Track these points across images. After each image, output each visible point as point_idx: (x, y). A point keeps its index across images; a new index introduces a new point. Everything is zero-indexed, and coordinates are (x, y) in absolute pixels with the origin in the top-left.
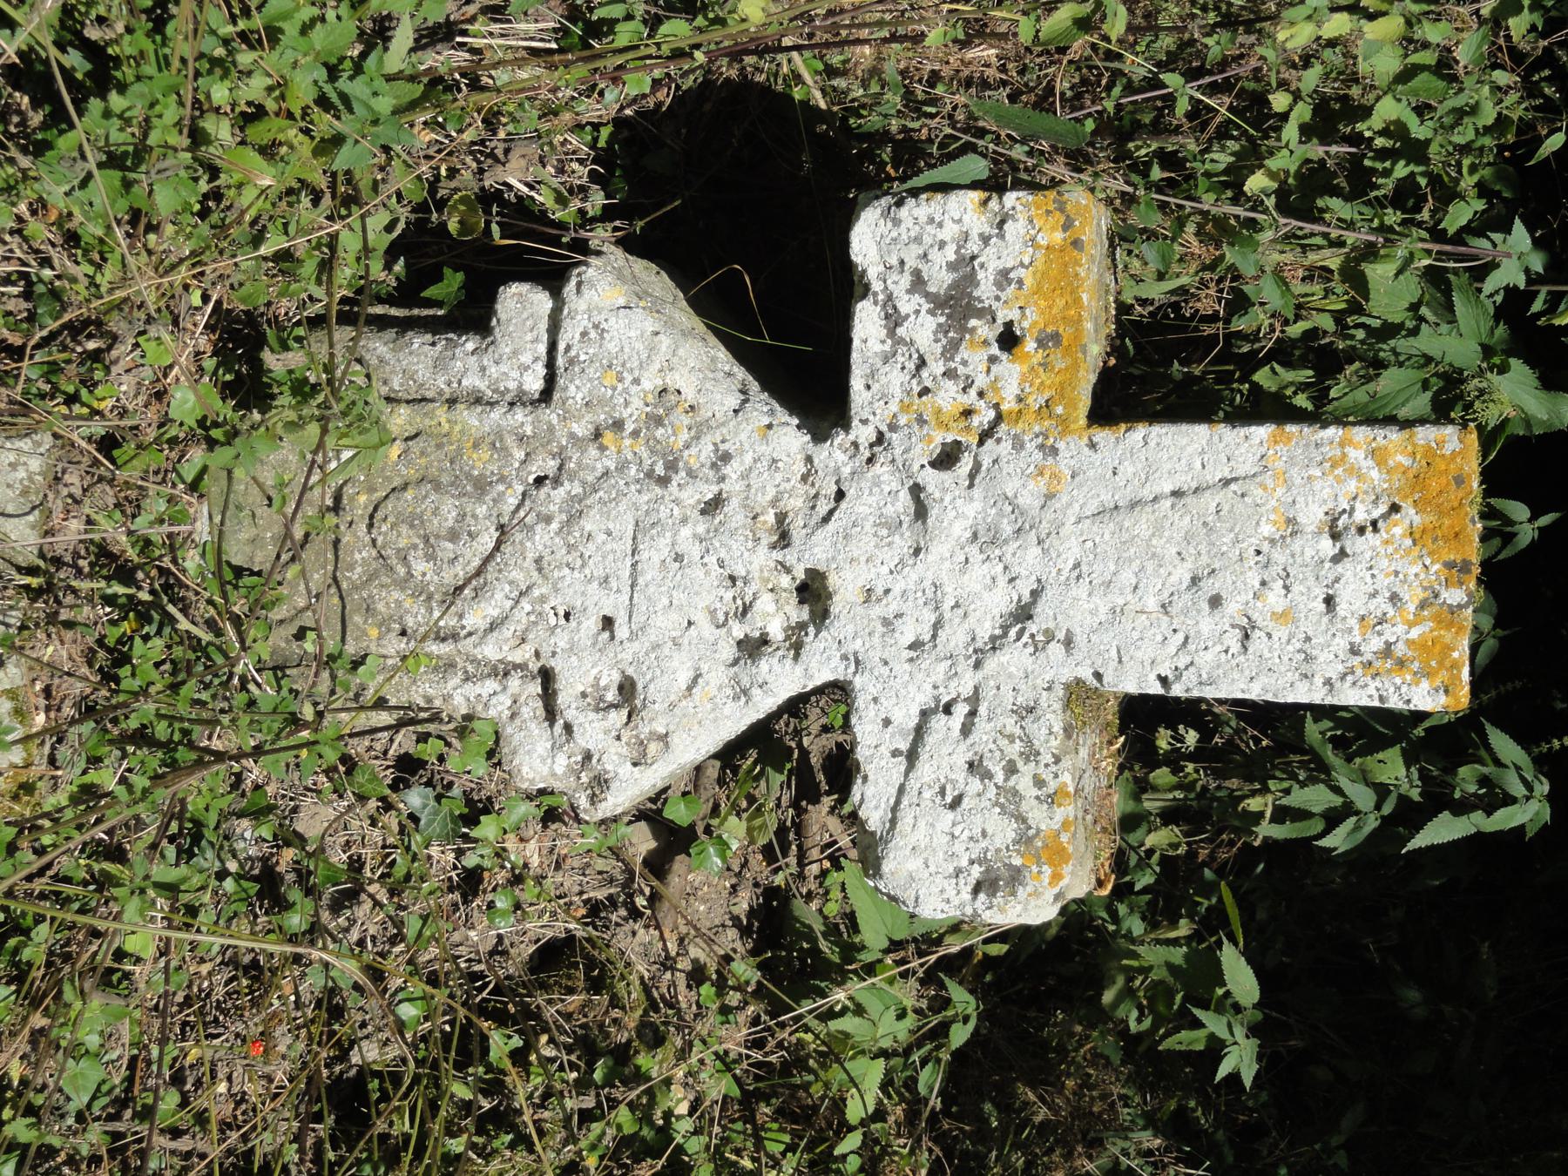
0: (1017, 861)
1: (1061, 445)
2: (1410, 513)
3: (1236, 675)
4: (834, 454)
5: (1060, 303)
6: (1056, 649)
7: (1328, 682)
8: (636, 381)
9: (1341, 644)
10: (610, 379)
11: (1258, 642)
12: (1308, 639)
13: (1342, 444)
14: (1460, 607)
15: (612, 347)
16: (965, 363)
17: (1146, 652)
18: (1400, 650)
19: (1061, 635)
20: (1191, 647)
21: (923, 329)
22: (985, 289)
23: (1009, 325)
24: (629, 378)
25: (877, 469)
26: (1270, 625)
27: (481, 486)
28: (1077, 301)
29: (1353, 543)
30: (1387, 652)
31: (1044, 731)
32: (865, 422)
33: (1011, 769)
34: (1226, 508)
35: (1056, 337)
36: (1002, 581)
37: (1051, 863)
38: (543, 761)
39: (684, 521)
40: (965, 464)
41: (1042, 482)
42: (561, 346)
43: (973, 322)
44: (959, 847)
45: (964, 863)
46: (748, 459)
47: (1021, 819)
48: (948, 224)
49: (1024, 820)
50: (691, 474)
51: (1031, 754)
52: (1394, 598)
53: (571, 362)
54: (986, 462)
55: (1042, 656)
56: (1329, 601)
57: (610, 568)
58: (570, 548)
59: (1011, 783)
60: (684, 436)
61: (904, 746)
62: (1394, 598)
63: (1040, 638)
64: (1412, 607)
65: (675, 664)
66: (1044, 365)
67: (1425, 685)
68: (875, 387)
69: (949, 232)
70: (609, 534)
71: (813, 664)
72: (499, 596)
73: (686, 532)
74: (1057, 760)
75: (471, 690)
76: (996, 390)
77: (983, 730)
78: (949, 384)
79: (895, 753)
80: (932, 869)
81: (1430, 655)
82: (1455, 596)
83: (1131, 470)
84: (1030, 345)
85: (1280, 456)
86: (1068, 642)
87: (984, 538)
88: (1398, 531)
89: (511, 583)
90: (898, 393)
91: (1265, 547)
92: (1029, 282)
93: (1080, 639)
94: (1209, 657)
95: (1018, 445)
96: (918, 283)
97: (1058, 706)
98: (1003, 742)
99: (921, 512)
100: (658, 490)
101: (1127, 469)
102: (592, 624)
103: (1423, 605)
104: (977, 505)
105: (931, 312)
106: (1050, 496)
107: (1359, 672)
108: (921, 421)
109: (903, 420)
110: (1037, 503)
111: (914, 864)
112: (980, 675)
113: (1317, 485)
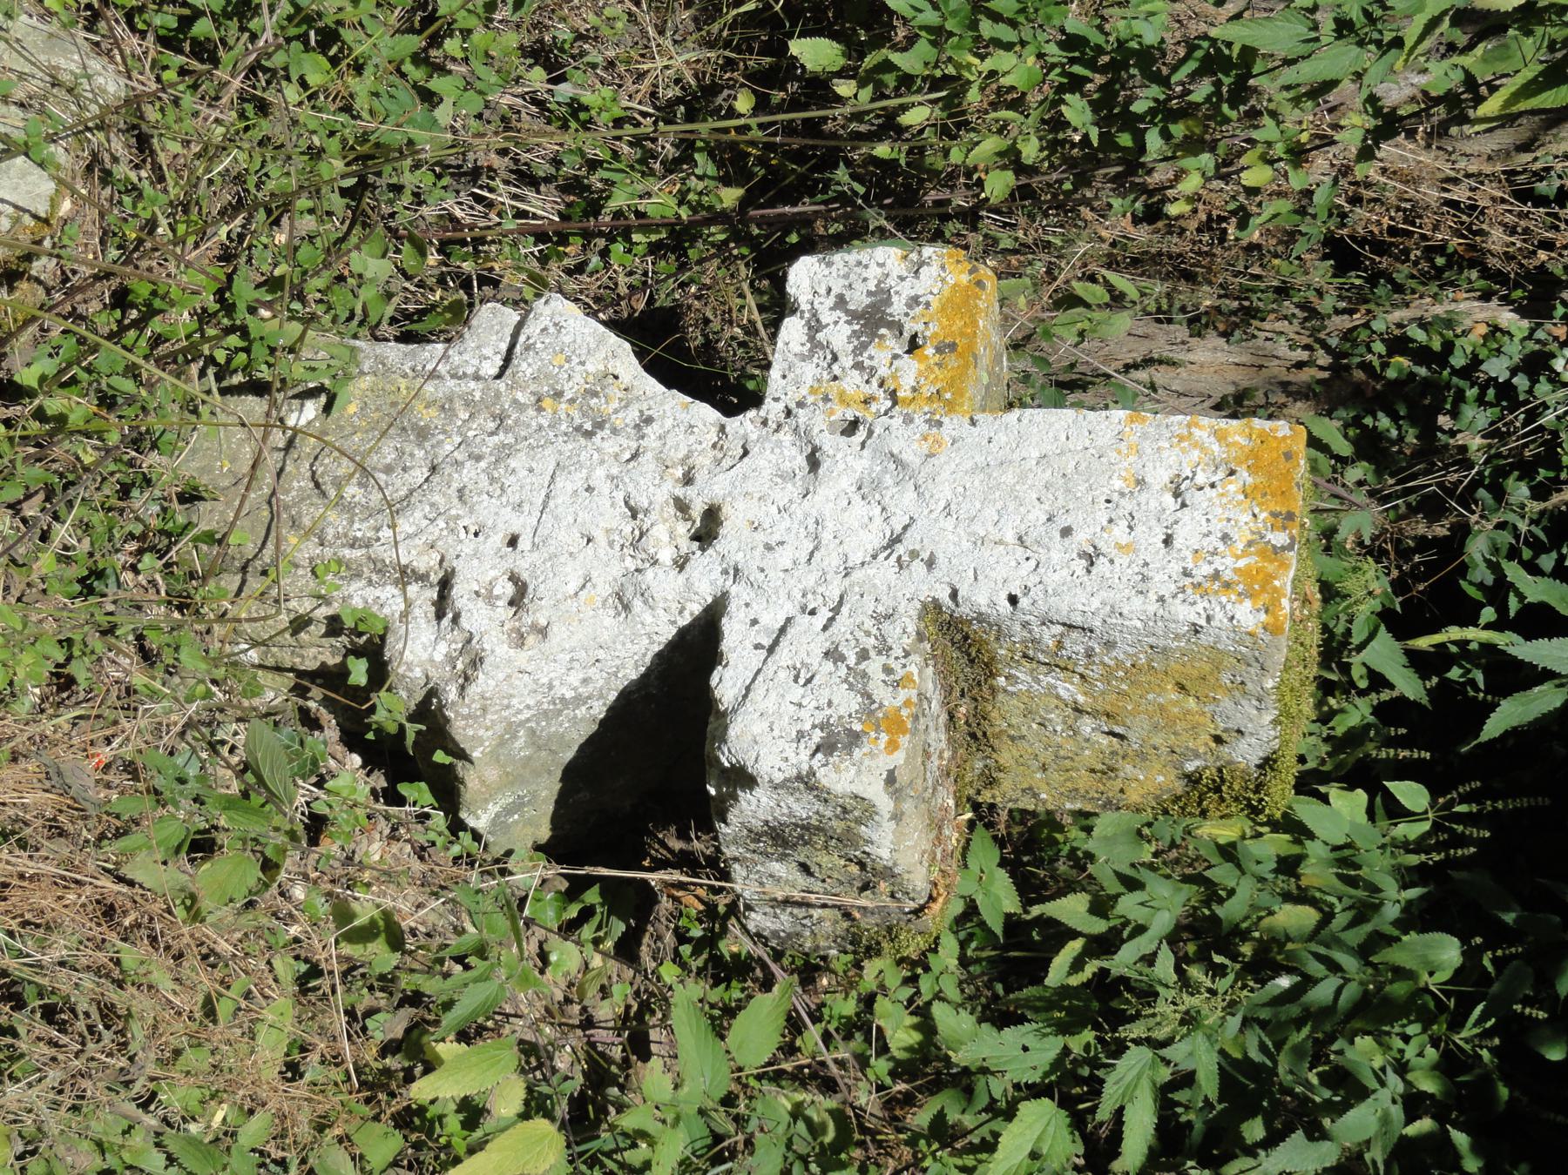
0: (857, 727)
1: (946, 420)
2: (1243, 475)
3: (1079, 590)
4: (744, 425)
5: (960, 323)
6: (918, 567)
7: (1161, 599)
8: (582, 363)
9: (1175, 568)
10: (561, 359)
11: (1102, 565)
12: (1146, 564)
13: (1189, 426)
14: (1283, 548)
15: (567, 339)
16: (871, 358)
17: (1001, 572)
18: (1227, 575)
19: (925, 555)
20: (1041, 570)
21: (839, 334)
22: (897, 308)
23: (914, 337)
24: (575, 360)
25: (781, 435)
26: (1113, 553)
27: (423, 434)
28: (974, 323)
29: (1191, 496)
30: (1216, 575)
31: (899, 630)
32: (776, 400)
33: (863, 655)
34: (1083, 465)
35: (953, 347)
36: (878, 520)
37: (888, 731)
38: (425, 648)
39: (602, 462)
40: (861, 434)
41: (925, 445)
42: (522, 339)
43: (883, 331)
44: (804, 714)
45: (807, 726)
46: (669, 423)
47: (868, 695)
48: (873, 266)
49: (869, 696)
50: (615, 431)
51: (884, 649)
52: (1225, 538)
53: (527, 348)
54: (878, 430)
55: (905, 573)
56: (1168, 541)
57: (528, 523)
58: (493, 480)
59: (862, 666)
60: (615, 404)
61: (767, 642)
62: (1225, 538)
63: (906, 558)
64: (1240, 546)
65: (568, 569)
66: (939, 365)
67: (1248, 604)
68: (790, 376)
69: (874, 272)
70: (531, 470)
71: (696, 574)
72: (418, 514)
73: (600, 472)
74: (907, 654)
75: (371, 593)
76: (894, 377)
77: (843, 623)
78: (856, 373)
79: (758, 646)
80: (776, 733)
81: (1255, 585)
82: (1279, 538)
83: (1004, 439)
84: (929, 351)
85: (1134, 432)
86: (930, 563)
87: (866, 489)
88: (1232, 488)
89: (432, 505)
90: (809, 382)
91: (1115, 497)
92: (935, 305)
93: (941, 560)
94: (1056, 577)
95: (908, 420)
96: (841, 302)
97: (914, 613)
98: (860, 634)
99: (814, 463)
100: (583, 441)
101: (1002, 438)
102: (498, 539)
103: (1250, 544)
104: (865, 463)
105: (849, 323)
106: (930, 455)
107: (1189, 591)
108: (826, 399)
109: (810, 400)
110: (918, 461)
111: (759, 727)
112: (847, 582)
113: (1165, 454)
